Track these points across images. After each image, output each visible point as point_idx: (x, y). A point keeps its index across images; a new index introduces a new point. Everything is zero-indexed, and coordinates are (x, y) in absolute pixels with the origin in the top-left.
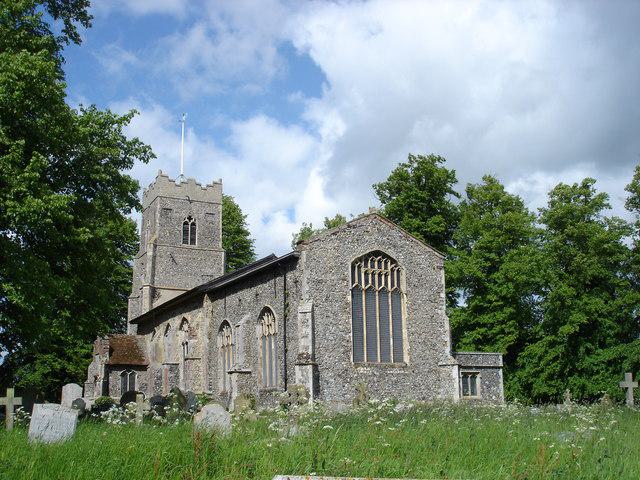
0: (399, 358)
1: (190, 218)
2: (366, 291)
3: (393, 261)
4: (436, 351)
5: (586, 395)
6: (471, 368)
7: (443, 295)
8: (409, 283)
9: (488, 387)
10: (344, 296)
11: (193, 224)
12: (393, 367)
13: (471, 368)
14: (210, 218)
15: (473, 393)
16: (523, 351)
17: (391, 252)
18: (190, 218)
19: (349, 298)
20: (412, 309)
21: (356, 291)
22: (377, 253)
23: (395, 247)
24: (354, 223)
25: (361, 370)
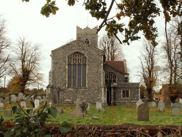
0: (84, 85)
1: (87, 40)
2: (73, 65)
3: (83, 55)
4: (98, 83)
5: (100, 100)
6: (126, 88)
7: (102, 64)
8: (89, 61)
9: (133, 95)
10: (65, 67)
11: (88, 42)
12: (81, 88)
13: (126, 88)
14: (93, 39)
15: (128, 96)
16: (37, 89)
17: (82, 52)
18: (87, 40)
19: (67, 67)
20: (90, 69)
21: (69, 65)
22: (77, 52)
23: (84, 50)
24: (69, 44)
25: (70, 89)
